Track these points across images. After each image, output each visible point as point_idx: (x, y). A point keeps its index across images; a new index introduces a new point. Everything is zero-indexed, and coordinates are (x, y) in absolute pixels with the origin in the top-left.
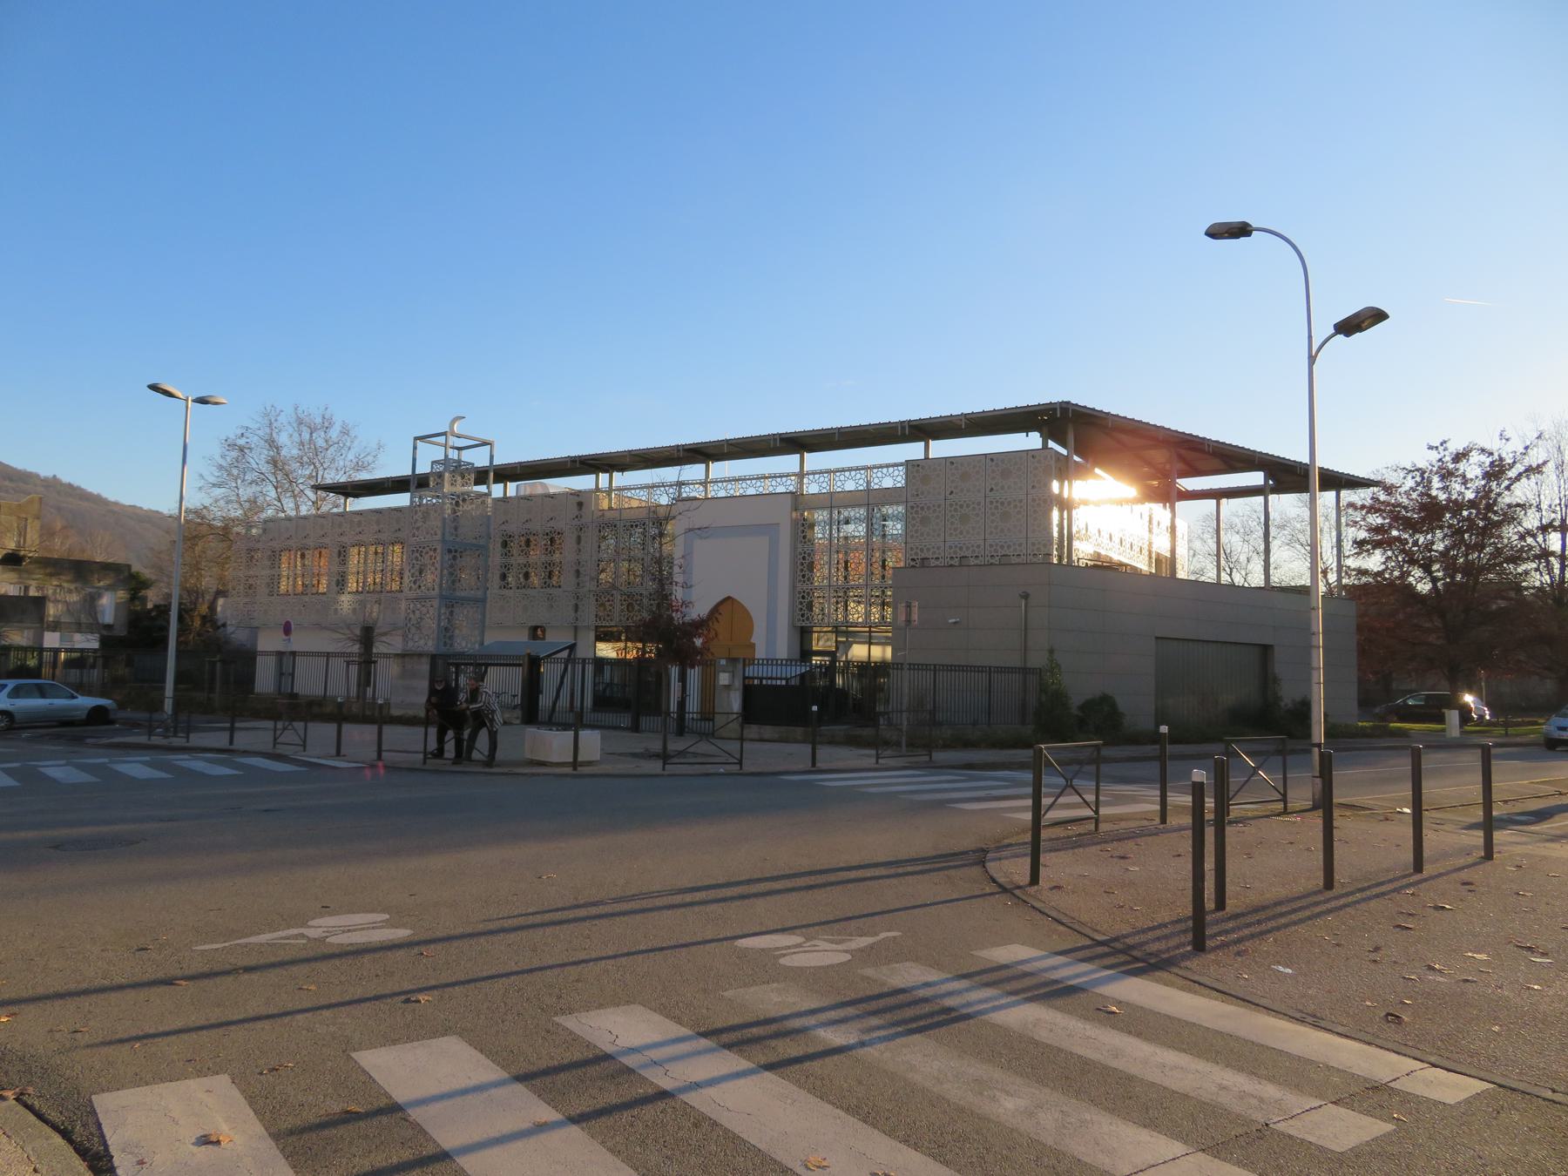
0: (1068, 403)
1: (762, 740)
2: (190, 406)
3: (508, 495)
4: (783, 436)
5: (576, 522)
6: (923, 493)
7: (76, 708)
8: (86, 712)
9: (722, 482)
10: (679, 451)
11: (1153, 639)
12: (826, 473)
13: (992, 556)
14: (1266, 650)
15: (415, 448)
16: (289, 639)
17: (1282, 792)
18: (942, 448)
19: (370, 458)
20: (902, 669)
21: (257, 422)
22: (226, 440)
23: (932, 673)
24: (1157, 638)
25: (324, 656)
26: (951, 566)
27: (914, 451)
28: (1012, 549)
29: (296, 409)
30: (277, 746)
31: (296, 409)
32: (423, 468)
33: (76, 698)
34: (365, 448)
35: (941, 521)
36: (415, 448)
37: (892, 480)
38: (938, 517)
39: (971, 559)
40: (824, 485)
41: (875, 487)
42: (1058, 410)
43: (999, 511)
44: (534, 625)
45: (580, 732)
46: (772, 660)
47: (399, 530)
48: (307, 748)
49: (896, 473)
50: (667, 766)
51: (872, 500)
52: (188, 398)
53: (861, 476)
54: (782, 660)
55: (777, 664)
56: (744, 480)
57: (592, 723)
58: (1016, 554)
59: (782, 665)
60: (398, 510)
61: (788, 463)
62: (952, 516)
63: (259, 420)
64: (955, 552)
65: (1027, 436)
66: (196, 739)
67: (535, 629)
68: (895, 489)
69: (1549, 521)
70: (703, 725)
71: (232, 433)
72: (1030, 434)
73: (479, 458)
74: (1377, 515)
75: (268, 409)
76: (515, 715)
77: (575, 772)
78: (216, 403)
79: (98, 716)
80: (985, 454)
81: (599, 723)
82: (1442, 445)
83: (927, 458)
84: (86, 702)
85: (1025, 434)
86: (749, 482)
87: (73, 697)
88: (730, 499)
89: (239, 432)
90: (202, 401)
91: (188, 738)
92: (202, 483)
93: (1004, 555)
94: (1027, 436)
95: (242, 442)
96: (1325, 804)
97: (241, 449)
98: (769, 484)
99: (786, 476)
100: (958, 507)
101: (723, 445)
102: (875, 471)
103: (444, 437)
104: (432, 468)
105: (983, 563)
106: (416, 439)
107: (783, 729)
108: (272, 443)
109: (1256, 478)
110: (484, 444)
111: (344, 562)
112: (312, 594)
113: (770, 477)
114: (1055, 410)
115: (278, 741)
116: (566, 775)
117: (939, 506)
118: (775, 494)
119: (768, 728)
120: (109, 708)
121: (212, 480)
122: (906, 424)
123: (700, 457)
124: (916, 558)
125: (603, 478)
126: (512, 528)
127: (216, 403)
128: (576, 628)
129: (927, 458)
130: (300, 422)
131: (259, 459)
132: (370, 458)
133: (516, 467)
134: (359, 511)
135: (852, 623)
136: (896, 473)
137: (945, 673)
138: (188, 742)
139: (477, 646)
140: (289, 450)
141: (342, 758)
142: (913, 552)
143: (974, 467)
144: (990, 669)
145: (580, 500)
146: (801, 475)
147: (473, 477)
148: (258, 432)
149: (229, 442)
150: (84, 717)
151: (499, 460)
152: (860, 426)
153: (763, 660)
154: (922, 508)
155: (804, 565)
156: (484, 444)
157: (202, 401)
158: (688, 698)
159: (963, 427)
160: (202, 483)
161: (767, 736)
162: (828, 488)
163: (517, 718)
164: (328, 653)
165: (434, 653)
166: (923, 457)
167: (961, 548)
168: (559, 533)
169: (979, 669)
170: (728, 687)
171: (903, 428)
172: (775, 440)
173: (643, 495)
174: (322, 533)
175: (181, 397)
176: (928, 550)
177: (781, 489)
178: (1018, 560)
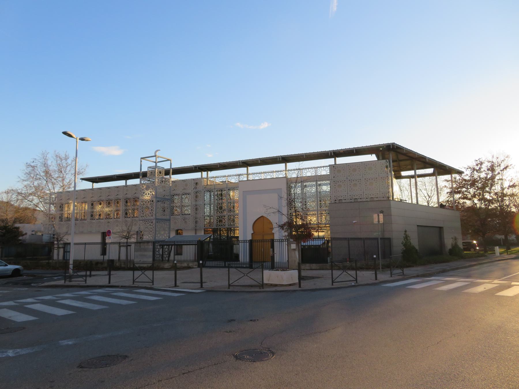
0: (394, 143)
1: (311, 269)
2: (78, 141)
3: (94, 188)
4: (282, 157)
5: (195, 190)
6: (338, 176)
7: (8, 270)
8: (11, 271)
9: (268, 173)
10: (115, 176)
11: (416, 226)
12: (314, 168)
13: (383, 197)
14: (441, 228)
15: (141, 161)
16: (110, 237)
17: (355, 278)
18: (341, 160)
19: (83, 170)
20: (247, 242)
21: (39, 157)
22: (27, 164)
23: (84, 245)
24: (418, 226)
25: (84, 244)
26: (367, 201)
27: (331, 161)
28: (358, 196)
29: (55, 152)
30: (135, 283)
31: (55, 152)
32: (145, 169)
33: (8, 266)
34: (82, 166)
35: (349, 186)
36: (141, 161)
37: (325, 172)
38: (344, 185)
39: (359, 200)
40: (313, 173)
41: (319, 175)
42: (304, 156)
43: (358, 184)
44: (177, 229)
45: (177, 271)
46: (245, 241)
47: (69, 199)
48: (154, 283)
49: (312, 171)
50: (334, 283)
51: (317, 179)
52: (77, 138)
53: (296, 172)
54: (241, 241)
55: (278, 241)
56: (242, 175)
57: (217, 266)
58: (344, 199)
59: (280, 241)
60: (135, 185)
61: (281, 166)
62: (350, 184)
63: (40, 156)
64: (352, 197)
65: (372, 156)
66: (90, 281)
67: (177, 231)
68: (327, 175)
69: (513, 184)
70: (266, 264)
71: (29, 161)
72: (372, 155)
73: (166, 166)
74: (455, 183)
75: (44, 152)
76: (195, 264)
77: (300, 289)
78: (87, 140)
79: (16, 273)
80: (346, 163)
81: (220, 266)
82: (479, 160)
83: (335, 164)
84: (11, 267)
85: (371, 155)
86: (220, 178)
87: (6, 265)
88: (252, 181)
89: (32, 161)
90: (82, 139)
91: (86, 281)
92: (19, 180)
93: (371, 198)
94: (372, 156)
95: (33, 164)
96: (110, 275)
97: (33, 167)
98: (276, 174)
99: (305, 169)
100: (360, 182)
101: (258, 160)
102: (304, 170)
103: (155, 157)
104: (148, 169)
105: (348, 202)
106: (142, 158)
107: (321, 265)
108: (45, 165)
109: (430, 171)
110: (168, 160)
111: (62, 210)
112: (97, 219)
113: (252, 174)
114: (303, 156)
115: (135, 281)
116: (295, 291)
117: (345, 181)
118: (266, 179)
119: (314, 264)
120: (21, 269)
121: (23, 178)
122: (133, 174)
123: (245, 165)
124: (336, 199)
125: (204, 174)
126: (129, 196)
127: (87, 140)
128: (196, 230)
129: (335, 164)
130: (57, 156)
131: (40, 170)
132: (83, 170)
133: (218, 165)
134: (100, 188)
135: (312, 224)
136: (312, 171)
137: (259, 243)
138: (86, 283)
139: (167, 238)
140: (53, 166)
141: (177, 287)
142: (351, 197)
143: (358, 167)
144: (349, 239)
145: (196, 182)
146: (248, 174)
147: (148, 175)
148: (40, 160)
149: (28, 164)
150: (11, 274)
151: (174, 166)
152: (314, 152)
153: (261, 240)
154: (338, 182)
155: (291, 202)
156: (168, 160)
157: (82, 139)
158: (275, 255)
159: (133, 176)
160: (19, 180)
161: (313, 268)
162: (315, 174)
163: (196, 265)
164: (85, 243)
165: (154, 241)
166: (334, 164)
167: (339, 197)
168: (189, 194)
169: (345, 239)
170: (294, 250)
171: (331, 153)
172: (240, 163)
173: (224, 179)
174: (68, 198)
175: (75, 137)
176: (373, 194)
177: (281, 176)
178: (377, 199)
